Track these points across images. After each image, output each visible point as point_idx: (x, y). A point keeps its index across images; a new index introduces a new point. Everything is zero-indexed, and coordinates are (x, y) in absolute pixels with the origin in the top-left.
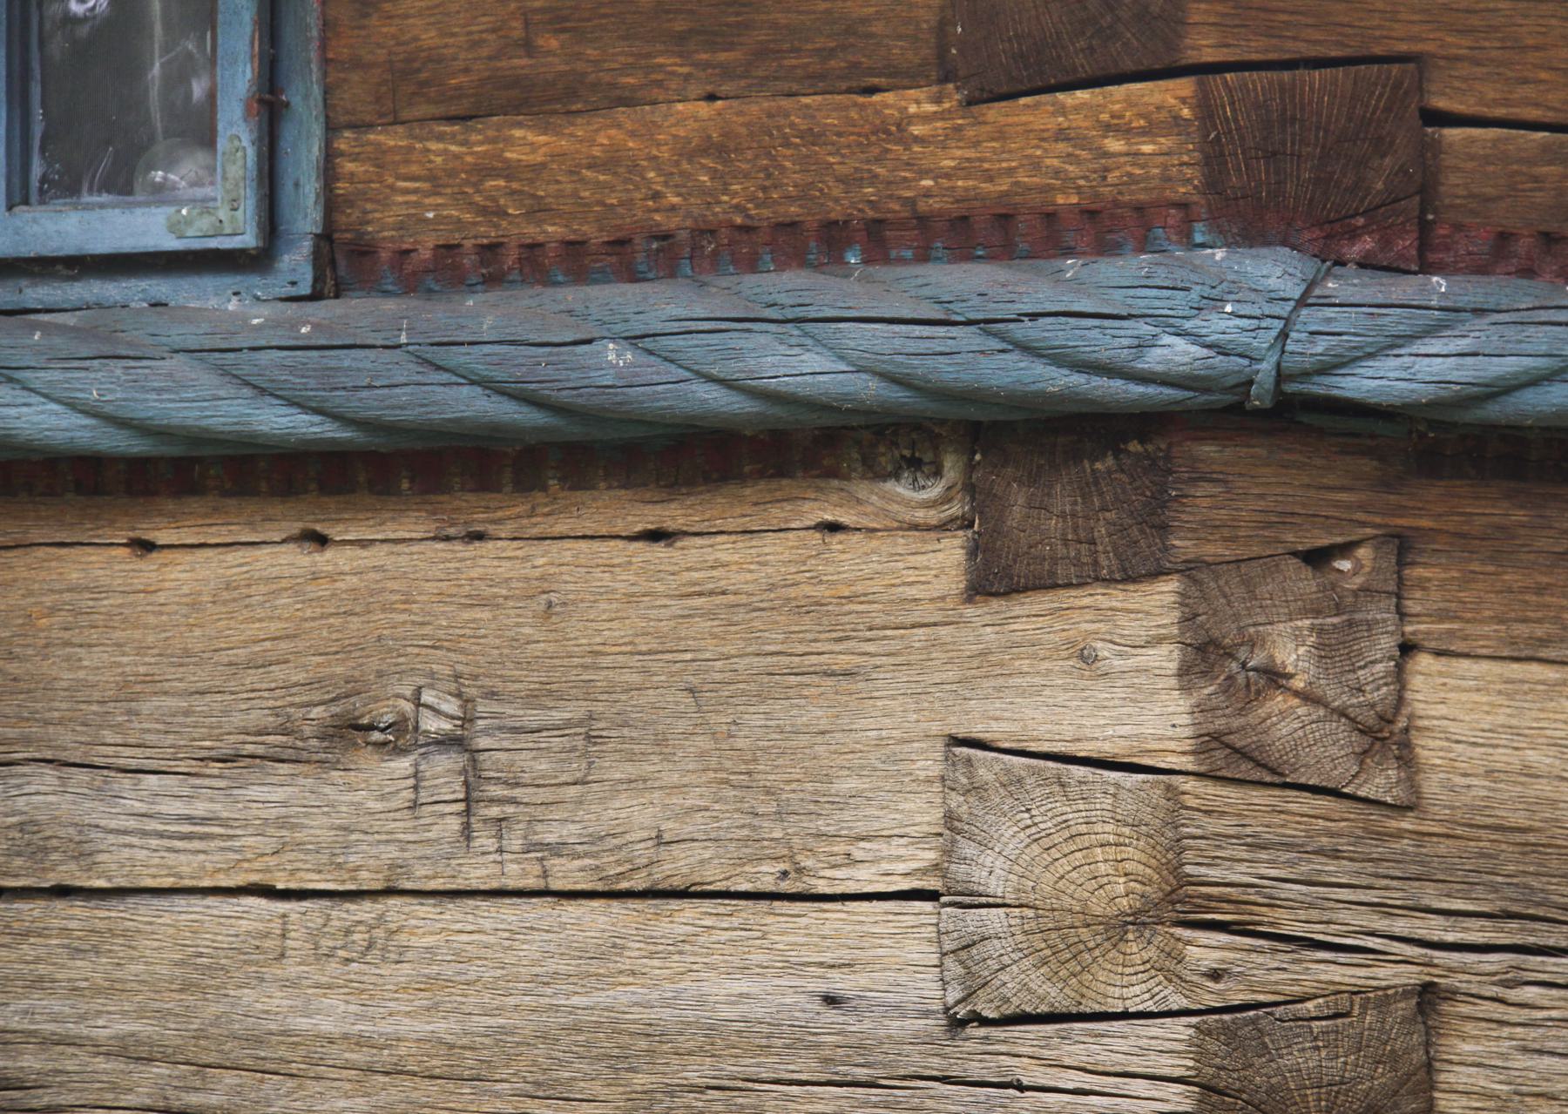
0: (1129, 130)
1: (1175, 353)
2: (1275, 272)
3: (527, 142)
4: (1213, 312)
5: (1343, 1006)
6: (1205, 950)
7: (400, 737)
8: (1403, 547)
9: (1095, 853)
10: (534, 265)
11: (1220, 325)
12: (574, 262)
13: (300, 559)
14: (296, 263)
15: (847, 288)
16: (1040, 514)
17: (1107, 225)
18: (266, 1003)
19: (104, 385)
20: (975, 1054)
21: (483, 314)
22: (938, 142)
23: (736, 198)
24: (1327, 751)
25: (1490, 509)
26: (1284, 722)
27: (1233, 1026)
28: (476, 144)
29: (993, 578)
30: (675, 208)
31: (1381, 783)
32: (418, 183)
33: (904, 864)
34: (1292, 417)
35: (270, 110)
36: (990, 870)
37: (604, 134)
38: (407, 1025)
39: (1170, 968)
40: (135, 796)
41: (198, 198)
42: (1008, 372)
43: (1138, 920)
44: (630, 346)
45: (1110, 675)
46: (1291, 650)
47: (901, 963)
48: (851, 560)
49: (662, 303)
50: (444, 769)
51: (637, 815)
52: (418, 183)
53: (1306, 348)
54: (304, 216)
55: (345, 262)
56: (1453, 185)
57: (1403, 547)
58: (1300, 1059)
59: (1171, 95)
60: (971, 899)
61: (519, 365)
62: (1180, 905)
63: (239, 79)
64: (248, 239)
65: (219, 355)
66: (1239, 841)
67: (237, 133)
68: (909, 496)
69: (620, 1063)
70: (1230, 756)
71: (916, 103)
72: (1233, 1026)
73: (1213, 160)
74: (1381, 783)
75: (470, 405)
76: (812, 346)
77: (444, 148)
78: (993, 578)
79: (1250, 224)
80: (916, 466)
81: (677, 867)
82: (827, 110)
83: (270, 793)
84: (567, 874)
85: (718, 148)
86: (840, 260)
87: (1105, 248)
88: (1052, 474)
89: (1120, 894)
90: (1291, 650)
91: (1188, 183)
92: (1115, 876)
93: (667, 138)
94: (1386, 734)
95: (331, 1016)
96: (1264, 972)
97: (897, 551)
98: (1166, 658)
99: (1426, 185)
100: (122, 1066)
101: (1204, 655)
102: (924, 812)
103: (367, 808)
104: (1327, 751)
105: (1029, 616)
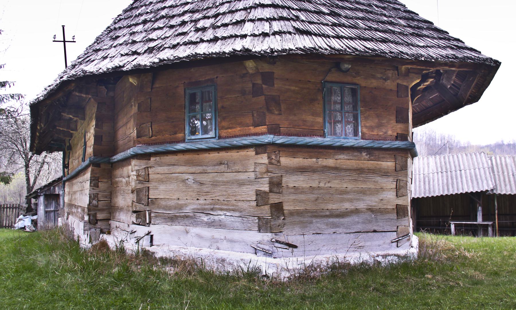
0: (263, 129)
1: (266, 141)
2: (272, 136)
3: (230, 130)
4: (268, 138)
5: (277, 177)
6: (269, 174)
7: (224, 164)
8: (279, 151)
9: (263, 169)
10: (230, 137)
11: (269, 139)
12: (233, 137)
13: (218, 154)
14: (217, 138)
15: (248, 138)
16: (259, 150)
17: (262, 134)
18: (217, 179)
19: (207, 145)
20: (257, 180)
21: (228, 140)
22: (252, 130)
23: (241, 133)
24: (276, 162)
25: (284, 149)
26: (273, 161)
27: (271, 178)
28: (227, 131)
29: (257, 154)
30: (238, 134)
31: (279, 164)
32: (224, 133)
33: (252, 170)
34: (273, 144)
35: (215, 129)
36: (257, 170)
37: (234, 130)
38: (225, 180)
39: (267, 175)
40: (209, 168)
41: (212, 134)
42: (257, 142)
43: (266, 172)
44: (236, 141)
45: (264, 159)
46: (273, 157)
47: (252, 175)
48: (249, 153)
49: (238, 139)
50: (226, 165)
51: (237, 168)
52: (224, 133)
53: (274, 140)
54: (217, 135)
55: (220, 138)
56: (281, 131)
57: (279, 151)
58: (275, 180)
59: (266, 127)
60: (256, 172)
61: (230, 143)
62: (268, 171)
63: (214, 128)
64: (326, 83)
65: (213, 143)
66: (271, 168)
67: (214, 131)
68: (252, 149)
69: (237, 181)
70: (270, 163)
71: (251, 127)
72: (271, 178)
73: (268, 130)
74: (279, 164)
75: (227, 145)
76: (246, 141)
77: (225, 131)
78: (257, 154)
79: (270, 134)
80: (252, 148)
81: (240, 170)
82: (246, 128)
83: (217, 167)
84: (233, 171)
85: (240, 130)
86: (58, 196)
87: (262, 135)
88: (260, 148)
89: (264, 171)
90: (273, 157)
91: (267, 131)
92: (264, 170)
93: (237, 130)
94: (279, 162)
95: (221, 179)
96: (272, 175)
97: (251, 152)
98: (266, 158)
99: (280, 131)
100: (323, 206)
101: (269, 158)
102: (253, 167)
103: (222, 168)
104: (276, 162)
105: (259, 156)
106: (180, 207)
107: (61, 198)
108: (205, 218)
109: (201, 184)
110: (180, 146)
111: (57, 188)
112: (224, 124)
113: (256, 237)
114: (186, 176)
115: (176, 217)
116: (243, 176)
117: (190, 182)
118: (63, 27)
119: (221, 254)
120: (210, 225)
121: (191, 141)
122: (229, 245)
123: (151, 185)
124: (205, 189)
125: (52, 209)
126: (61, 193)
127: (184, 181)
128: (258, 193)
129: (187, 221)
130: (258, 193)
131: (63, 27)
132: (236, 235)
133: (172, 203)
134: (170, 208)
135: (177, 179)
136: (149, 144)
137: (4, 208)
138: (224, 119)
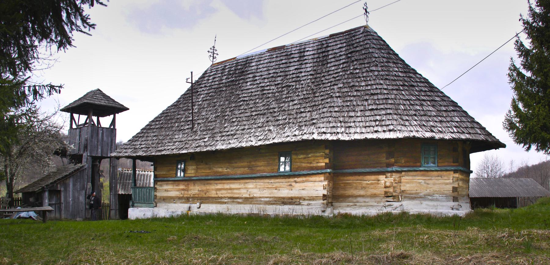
32: (440, 165)
86: (59, 192)
97: (452, 173)
106: (418, 193)
107: (62, 194)
108: (430, 198)
109: (428, 184)
110: (421, 169)
111: (59, 186)
112: (440, 161)
113: (452, 204)
114: (421, 181)
115: (416, 198)
116: (448, 181)
117: (423, 183)
118: (192, 73)
119: (440, 211)
120: (432, 200)
121: (424, 167)
122: (441, 207)
123: (402, 184)
124: (429, 186)
125: (53, 203)
126: (62, 189)
127: (420, 183)
128: (453, 188)
129: (420, 199)
130: (453, 188)
131: (192, 73)
132: (444, 204)
133: (414, 192)
134: (412, 194)
135: (416, 182)
136: (401, 166)
137: (16, 201)
138: (440, 159)
